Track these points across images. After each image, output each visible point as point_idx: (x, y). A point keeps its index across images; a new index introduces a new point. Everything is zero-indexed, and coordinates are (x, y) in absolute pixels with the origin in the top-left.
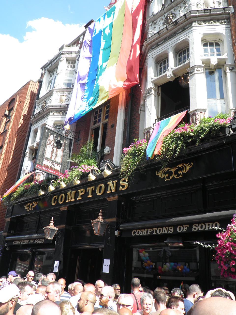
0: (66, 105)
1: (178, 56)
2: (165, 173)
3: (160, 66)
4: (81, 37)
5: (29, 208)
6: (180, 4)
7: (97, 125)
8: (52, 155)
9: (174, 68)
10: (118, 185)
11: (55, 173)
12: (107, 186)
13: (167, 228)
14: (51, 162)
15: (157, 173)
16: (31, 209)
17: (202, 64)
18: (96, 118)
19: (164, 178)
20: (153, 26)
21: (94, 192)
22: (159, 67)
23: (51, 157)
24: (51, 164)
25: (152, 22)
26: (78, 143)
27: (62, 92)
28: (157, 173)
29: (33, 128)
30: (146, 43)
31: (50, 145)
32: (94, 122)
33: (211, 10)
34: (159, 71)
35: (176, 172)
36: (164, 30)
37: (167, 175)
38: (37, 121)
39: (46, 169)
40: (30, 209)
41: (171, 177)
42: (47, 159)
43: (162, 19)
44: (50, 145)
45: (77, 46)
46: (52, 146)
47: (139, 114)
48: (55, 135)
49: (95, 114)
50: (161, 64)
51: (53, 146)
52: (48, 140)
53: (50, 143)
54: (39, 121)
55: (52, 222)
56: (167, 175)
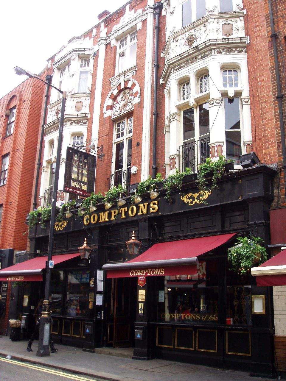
0: (84, 114)
1: (199, 81)
2: (189, 199)
3: (184, 88)
4: (94, 31)
5: (59, 227)
6: (200, 26)
7: (121, 139)
8: (78, 176)
9: (197, 96)
10: (148, 207)
11: (83, 193)
12: (138, 208)
13: (160, 269)
14: (78, 182)
15: (182, 198)
16: (61, 229)
17: (221, 97)
18: (118, 130)
19: (188, 203)
20: (175, 43)
21: (126, 213)
22: (182, 90)
23: (78, 178)
24: (78, 185)
25: (174, 39)
26: (102, 159)
27: (78, 97)
28: (182, 198)
29: (47, 139)
30: (168, 63)
31: (75, 166)
32: (117, 135)
33: (228, 39)
34: (182, 94)
35: (198, 198)
36: (185, 53)
37: (191, 200)
38: (52, 130)
39: (74, 191)
40: (60, 228)
41: (194, 202)
42: (75, 181)
43: (184, 38)
44: (75, 166)
45: (90, 39)
46: (77, 166)
47: (164, 134)
48: (79, 155)
49: (118, 127)
50: (183, 86)
51: (78, 166)
52: (73, 161)
53: (75, 163)
54: (54, 130)
55: (85, 242)
56: (191, 200)
